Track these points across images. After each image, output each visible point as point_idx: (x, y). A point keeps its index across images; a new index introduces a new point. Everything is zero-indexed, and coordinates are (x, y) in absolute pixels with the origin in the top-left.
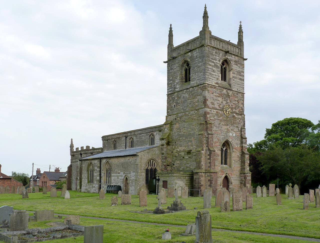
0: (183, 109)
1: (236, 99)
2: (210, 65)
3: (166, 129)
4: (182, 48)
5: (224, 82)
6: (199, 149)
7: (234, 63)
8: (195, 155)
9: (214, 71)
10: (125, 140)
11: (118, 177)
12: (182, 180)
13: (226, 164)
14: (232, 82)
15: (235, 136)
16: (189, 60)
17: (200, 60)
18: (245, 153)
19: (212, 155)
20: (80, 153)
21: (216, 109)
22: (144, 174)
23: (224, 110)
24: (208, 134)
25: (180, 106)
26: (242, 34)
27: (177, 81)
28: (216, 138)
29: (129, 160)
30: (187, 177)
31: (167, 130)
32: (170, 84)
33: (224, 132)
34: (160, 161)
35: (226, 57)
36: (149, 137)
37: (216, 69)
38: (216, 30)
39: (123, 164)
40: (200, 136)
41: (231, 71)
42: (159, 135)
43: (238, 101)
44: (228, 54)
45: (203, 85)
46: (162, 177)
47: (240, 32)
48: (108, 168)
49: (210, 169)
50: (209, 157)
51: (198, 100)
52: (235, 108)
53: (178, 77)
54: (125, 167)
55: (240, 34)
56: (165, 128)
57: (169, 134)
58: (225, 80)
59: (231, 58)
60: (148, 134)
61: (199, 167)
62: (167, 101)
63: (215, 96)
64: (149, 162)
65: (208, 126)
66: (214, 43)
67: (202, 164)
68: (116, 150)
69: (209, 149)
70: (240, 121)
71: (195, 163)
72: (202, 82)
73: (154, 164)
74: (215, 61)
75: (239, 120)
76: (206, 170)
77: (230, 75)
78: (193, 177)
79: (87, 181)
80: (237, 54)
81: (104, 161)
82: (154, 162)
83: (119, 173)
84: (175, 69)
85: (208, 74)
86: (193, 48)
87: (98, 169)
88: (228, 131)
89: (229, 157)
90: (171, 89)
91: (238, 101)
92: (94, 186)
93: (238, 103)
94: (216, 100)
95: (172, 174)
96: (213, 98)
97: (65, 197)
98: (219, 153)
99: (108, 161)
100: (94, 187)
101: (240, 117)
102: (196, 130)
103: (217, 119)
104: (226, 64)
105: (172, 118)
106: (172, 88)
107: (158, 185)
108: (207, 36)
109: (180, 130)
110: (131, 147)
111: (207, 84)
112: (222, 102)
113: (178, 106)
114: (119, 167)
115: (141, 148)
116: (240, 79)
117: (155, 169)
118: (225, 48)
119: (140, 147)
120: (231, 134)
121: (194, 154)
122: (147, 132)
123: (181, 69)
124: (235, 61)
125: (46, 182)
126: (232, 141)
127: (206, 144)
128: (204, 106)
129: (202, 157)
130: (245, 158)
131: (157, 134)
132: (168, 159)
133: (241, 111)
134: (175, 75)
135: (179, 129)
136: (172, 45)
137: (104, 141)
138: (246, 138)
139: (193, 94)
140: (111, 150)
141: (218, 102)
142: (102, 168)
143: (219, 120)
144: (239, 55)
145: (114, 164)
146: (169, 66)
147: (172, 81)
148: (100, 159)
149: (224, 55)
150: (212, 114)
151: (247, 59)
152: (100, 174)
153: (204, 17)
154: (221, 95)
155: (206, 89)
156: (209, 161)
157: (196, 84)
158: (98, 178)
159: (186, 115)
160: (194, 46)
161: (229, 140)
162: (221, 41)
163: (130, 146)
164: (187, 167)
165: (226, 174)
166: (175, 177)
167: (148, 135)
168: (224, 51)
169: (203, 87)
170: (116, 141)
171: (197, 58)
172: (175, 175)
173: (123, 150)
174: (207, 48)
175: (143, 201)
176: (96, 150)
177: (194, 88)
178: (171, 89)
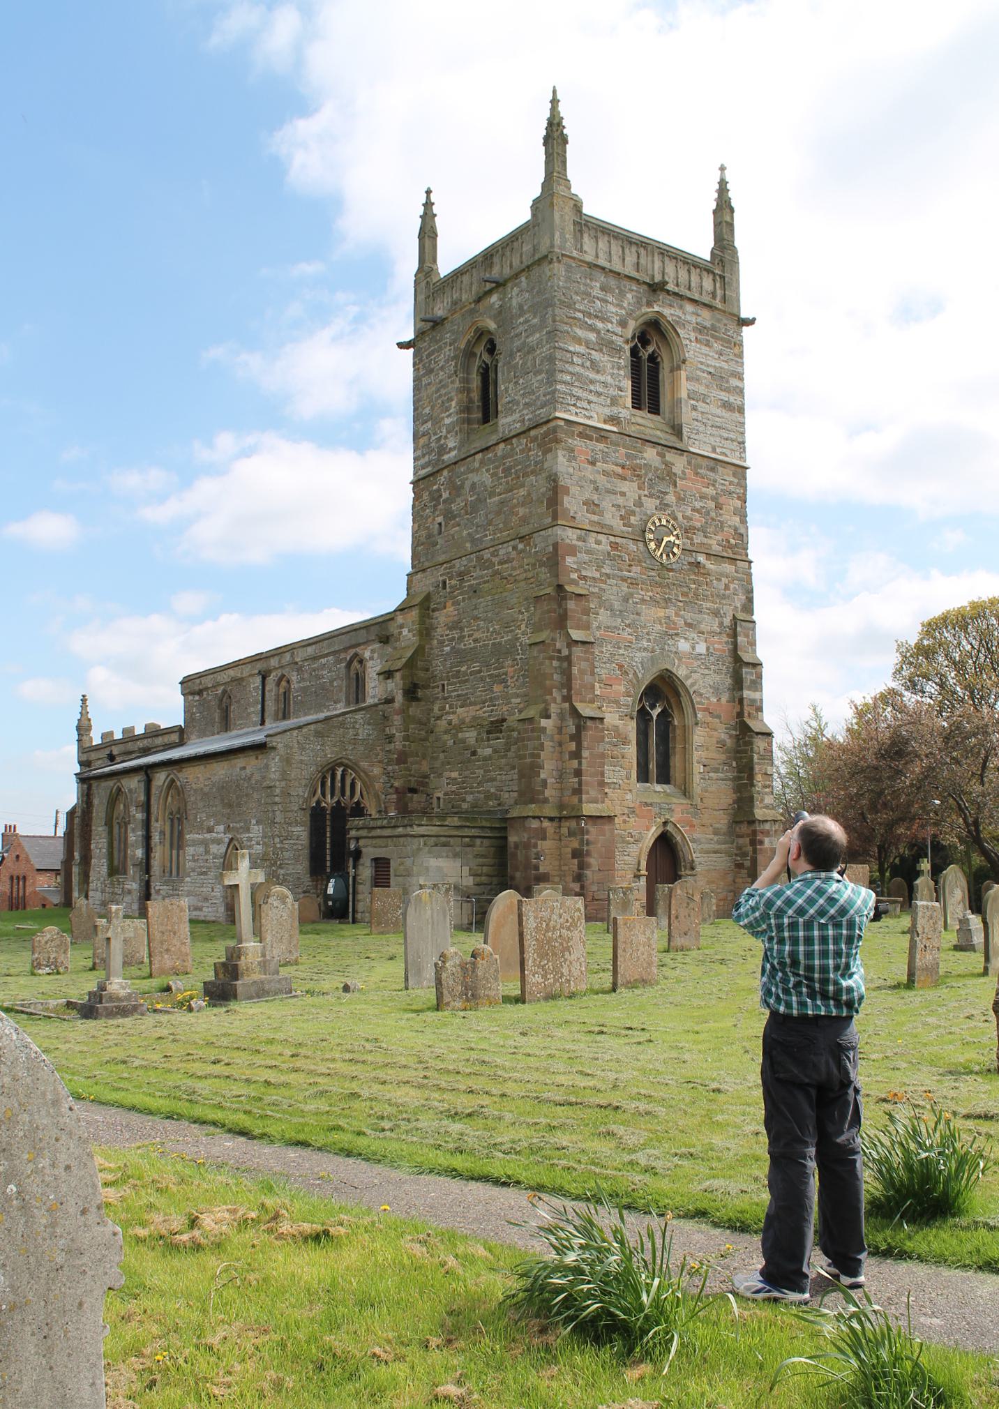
0: (473, 541)
1: (710, 491)
2: (578, 341)
3: (405, 632)
4: (466, 278)
6: (531, 712)
7: (693, 336)
9: (595, 366)
12: (456, 855)
13: (664, 778)
14: (687, 416)
15: (704, 651)
16: (492, 325)
19: (588, 736)
21: (607, 531)
22: (301, 833)
23: (651, 536)
25: (459, 525)
26: (728, 219)
27: (447, 421)
30: (478, 841)
32: (423, 435)
33: (648, 634)
34: (376, 771)
35: (656, 309)
36: (343, 671)
37: (606, 358)
38: (604, 194)
41: (679, 368)
43: (714, 499)
44: (662, 296)
45: (545, 428)
49: (580, 801)
50: (573, 746)
51: (529, 494)
52: (703, 530)
53: (454, 403)
55: (722, 216)
56: (401, 627)
58: (655, 409)
59: (680, 314)
60: (343, 655)
61: (529, 794)
64: (324, 778)
65: (571, 605)
66: (591, 249)
67: (544, 783)
69: (575, 712)
70: (727, 587)
73: (353, 785)
74: (600, 325)
75: (724, 580)
76: (561, 807)
77: (682, 386)
78: (505, 838)
79: (104, 870)
80: (706, 299)
81: (160, 778)
82: (351, 775)
83: (210, 830)
84: (442, 368)
86: (507, 272)
87: (140, 816)
88: (671, 634)
89: (679, 746)
90: (426, 459)
91: (714, 499)
93: (719, 507)
94: (608, 491)
95: (395, 827)
96: (593, 482)
98: (631, 728)
101: (728, 568)
103: (614, 577)
104: (655, 339)
106: (429, 453)
107: (354, 878)
108: (562, 217)
109: (462, 629)
111: (562, 423)
112: (639, 503)
116: (727, 406)
118: (650, 272)
120: (683, 646)
122: (337, 648)
123: (467, 370)
124: (701, 329)
126: (688, 677)
129: (542, 747)
132: (410, 760)
133: (733, 542)
134: (440, 396)
135: (455, 626)
137: (190, 698)
138: (757, 665)
139: (510, 468)
141: (621, 500)
142: (154, 809)
143: (624, 579)
144: (718, 303)
145: (195, 791)
146: (421, 360)
147: (429, 424)
148: (147, 771)
149: (644, 300)
150: (589, 552)
151: (754, 319)
152: (148, 838)
153: (547, 140)
154: (635, 471)
155: (557, 441)
156: (575, 763)
157: (518, 425)
158: (139, 853)
159: (484, 564)
160: (511, 266)
161: (674, 670)
162: (631, 243)
163: (281, 715)
164: (489, 796)
165: (665, 823)
166: (422, 840)
167: (340, 661)
168: (645, 283)
169: (545, 432)
171: (522, 311)
174: (559, 269)
175: (168, 950)
176: (160, 738)
177: (514, 441)
178: (426, 459)
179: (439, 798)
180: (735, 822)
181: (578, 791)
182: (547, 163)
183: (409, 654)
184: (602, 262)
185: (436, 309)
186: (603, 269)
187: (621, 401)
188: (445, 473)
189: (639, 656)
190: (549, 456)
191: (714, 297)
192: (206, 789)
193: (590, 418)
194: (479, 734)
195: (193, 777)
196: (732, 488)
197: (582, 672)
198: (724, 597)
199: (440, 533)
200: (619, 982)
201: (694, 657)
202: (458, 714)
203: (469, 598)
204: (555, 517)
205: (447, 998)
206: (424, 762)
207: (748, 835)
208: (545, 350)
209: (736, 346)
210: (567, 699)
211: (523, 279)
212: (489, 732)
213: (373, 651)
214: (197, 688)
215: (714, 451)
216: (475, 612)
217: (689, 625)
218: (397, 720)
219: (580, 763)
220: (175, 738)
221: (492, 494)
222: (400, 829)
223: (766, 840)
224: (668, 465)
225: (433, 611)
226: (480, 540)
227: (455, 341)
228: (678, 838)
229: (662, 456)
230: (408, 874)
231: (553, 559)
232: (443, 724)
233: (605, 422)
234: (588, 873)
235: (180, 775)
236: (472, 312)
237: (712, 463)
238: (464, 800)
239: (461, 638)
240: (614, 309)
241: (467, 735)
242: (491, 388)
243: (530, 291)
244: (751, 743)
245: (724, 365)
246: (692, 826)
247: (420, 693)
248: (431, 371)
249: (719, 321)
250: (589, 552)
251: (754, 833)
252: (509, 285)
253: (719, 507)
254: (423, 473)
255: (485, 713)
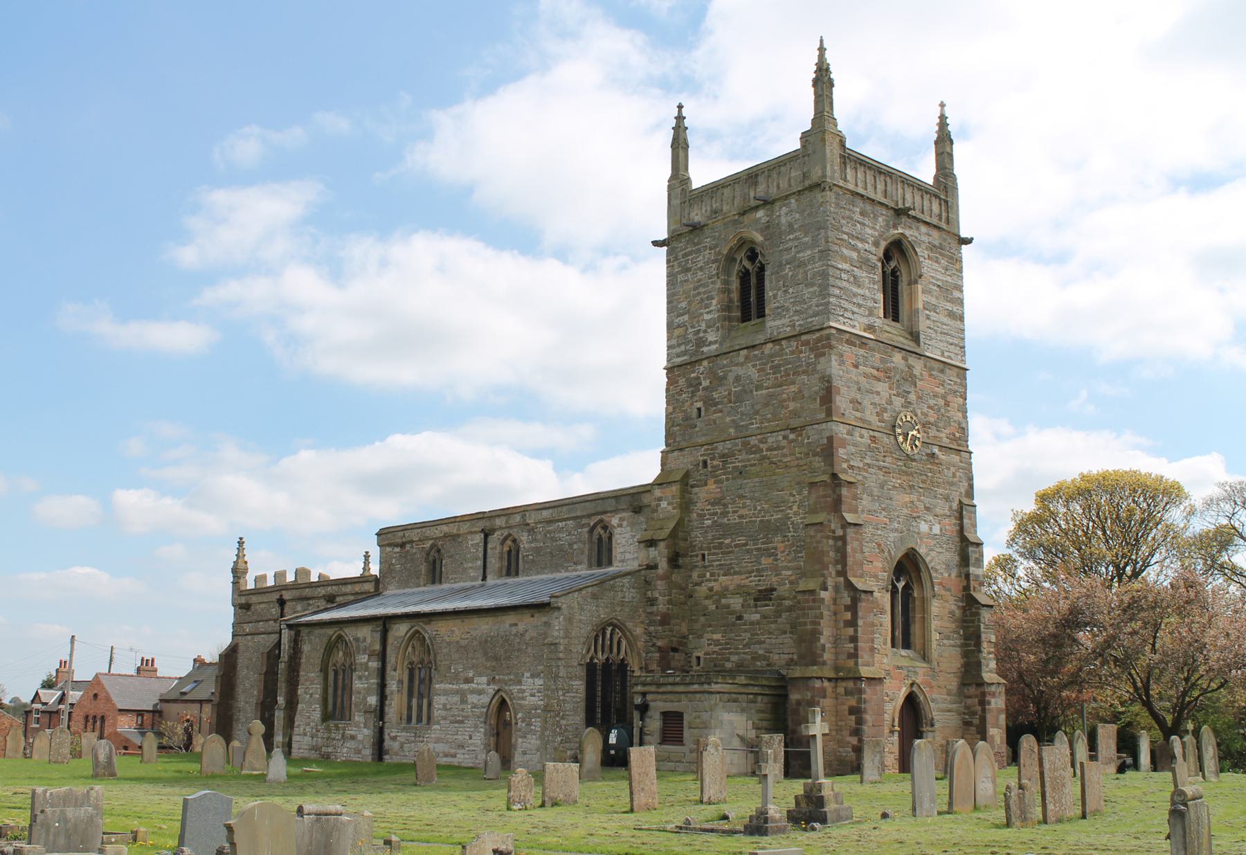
0: (737, 427)
1: (940, 390)
2: (845, 259)
3: (664, 504)
4: (727, 191)
5: (893, 323)
6: (811, 585)
8: (790, 609)
9: (857, 281)
10: (482, 544)
11: (463, 696)
12: (743, 710)
13: (907, 645)
14: (923, 325)
15: (938, 532)
16: (759, 238)
17: (806, 239)
18: (978, 603)
19: (862, 606)
20: (276, 596)
21: (865, 425)
22: (579, 686)
23: (899, 431)
24: (846, 525)
27: (707, 317)
28: (871, 541)
29: (516, 625)
30: (759, 698)
31: (670, 508)
32: (679, 326)
34: (639, 631)
35: (900, 231)
37: (864, 274)
39: (486, 644)
40: (812, 531)
41: (916, 282)
42: (632, 525)
44: (904, 219)
45: (818, 335)
46: (660, 696)
47: (944, 142)
48: (415, 659)
49: (856, 664)
50: (848, 616)
51: (800, 391)
53: (714, 302)
54: (497, 656)
56: (660, 499)
57: (677, 524)
58: (896, 318)
60: (584, 521)
61: (810, 656)
62: (667, 390)
63: (866, 375)
65: (844, 491)
66: (854, 180)
67: (824, 646)
68: (436, 587)
69: (850, 586)
70: (954, 475)
71: (787, 639)
72: (816, 321)
73: (619, 642)
74: (860, 245)
76: (837, 669)
77: (921, 297)
78: (786, 696)
79: (317, 715)
80: (935, 221)
82: (618, 634)
83: (468, 681)
84: (701, 269)
85: (837, 292)
89: (918, 616)
90: (683, 348)
91: (944, 397)
92: (352, 733)
95: (702, 684)
97: (270, 776)
98: (886, 599)
99: (417, 632)
100: (353, 738)
101: (955, 458)
102: (790, 508)
105: (684, 461)
106: (686, 344)
107: (641, 730)
108: (832, 152)
109: (725, 506)
110: (508, 574)
111: (834, 331)
113: (715, 412)
114: (470, 655)
115: (554, 581)
116: (951, 315)
117: (623, 665)
119: (550, 576)
120: (924, 527)
121: (787, 603)
122: (579, 514)
123: (727, 272)
124: (932, 247)
125: (103, 718)
127: (837, 562)
128: (823, 415)
130: (979, 620)
131: (625, 523)
132: (673, 622)
134: (699, 294)
136: (687, 181)
137: (388, 549)
139: (779, 366)
140: (419, 586)
141: (877, 400)
143: (880, 468)
144: (944, 225)
145: (449, 643)
146: (676, 259)
147: (686, 317)
148: (385, 622)
150: (855, 445)
152: (382, 686)
153: (816, 83)
154: (886, 373)
155: (831, 347)
156: (851, 631)
157: (788, 329)
158: (373, 700)
159: (751, 450)
160: (778, 187)
163: (504, 572)
164: (756, 657)
165: (912, 685)
167: (583, 526)
169: (819, 340)
170: (439, 551)
172: (715, 687)
173: (473, 587)
174: (830, 196)
176: (350, 587)
177: (783, 342)
178: (683, 348)
179: (698, 658)
180: (963, 684)
181: (854, 655)
182: (816, 102)
183: (672, 525)
184: (860, 190)
185: (693, 214)
186: (862, 196)
187: (876, 311)
188: (705, 363)
189: (893, 536)
190: (822, 360)
191: (940, 219)
192: (464, 643)
193: (854, 327)
194: (745, 601)
195: (441, 629)
196: (956, 387)
197: (854, 550)
198: (952, 484)
199: (700, 416)
200: (1088, 811)
201: (931, 538)
202: (721, 582)
203: (734, 479)
204: (829, 413)
205: (1013, 820)
206: (684, 624)
207: (976, 696)
208: (818, 266)
209: (956, 261)
210: (842, 573)
211: (793, 201)
212: (756, 600)
213: (621, 519)
214: (400, 541)
215: (943, 355)
216: (741, 492)
217: (927, 509)
218: (661, 585)
219: (856, 631)
220: (369, 587)
221: (758, 388)
222: (696, 686)
223: (993, 701)
224: (910, 367)
225: (692, 487)
226: (746, 427)
227: (716, 246)
228: (921, 698)
229: (905, 359)
230: (705, 726)
231: (828, 450)
232: (703, 590)
233: (865, 331)
234: (865, 727)
235: (427, 627)
236: (735, 222)
237: (942, 365)
238: (728, 660)
239: (725, 514)
240: (870, 231)
241: (732, 601)
242: (753, 292)
243: (802, 212)
244: (978, 614)
245: (949, 279)
246: (931, 687)
247: (681, 561)
248: (688, 270)
249: (945, 240)
250: (855, 445)
251: (983, 694)
252: (778, 204)
253: (947, 404)
254: (678, 360)
255: (752, 582)
